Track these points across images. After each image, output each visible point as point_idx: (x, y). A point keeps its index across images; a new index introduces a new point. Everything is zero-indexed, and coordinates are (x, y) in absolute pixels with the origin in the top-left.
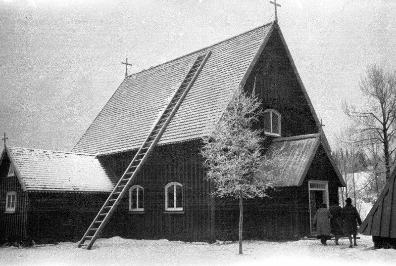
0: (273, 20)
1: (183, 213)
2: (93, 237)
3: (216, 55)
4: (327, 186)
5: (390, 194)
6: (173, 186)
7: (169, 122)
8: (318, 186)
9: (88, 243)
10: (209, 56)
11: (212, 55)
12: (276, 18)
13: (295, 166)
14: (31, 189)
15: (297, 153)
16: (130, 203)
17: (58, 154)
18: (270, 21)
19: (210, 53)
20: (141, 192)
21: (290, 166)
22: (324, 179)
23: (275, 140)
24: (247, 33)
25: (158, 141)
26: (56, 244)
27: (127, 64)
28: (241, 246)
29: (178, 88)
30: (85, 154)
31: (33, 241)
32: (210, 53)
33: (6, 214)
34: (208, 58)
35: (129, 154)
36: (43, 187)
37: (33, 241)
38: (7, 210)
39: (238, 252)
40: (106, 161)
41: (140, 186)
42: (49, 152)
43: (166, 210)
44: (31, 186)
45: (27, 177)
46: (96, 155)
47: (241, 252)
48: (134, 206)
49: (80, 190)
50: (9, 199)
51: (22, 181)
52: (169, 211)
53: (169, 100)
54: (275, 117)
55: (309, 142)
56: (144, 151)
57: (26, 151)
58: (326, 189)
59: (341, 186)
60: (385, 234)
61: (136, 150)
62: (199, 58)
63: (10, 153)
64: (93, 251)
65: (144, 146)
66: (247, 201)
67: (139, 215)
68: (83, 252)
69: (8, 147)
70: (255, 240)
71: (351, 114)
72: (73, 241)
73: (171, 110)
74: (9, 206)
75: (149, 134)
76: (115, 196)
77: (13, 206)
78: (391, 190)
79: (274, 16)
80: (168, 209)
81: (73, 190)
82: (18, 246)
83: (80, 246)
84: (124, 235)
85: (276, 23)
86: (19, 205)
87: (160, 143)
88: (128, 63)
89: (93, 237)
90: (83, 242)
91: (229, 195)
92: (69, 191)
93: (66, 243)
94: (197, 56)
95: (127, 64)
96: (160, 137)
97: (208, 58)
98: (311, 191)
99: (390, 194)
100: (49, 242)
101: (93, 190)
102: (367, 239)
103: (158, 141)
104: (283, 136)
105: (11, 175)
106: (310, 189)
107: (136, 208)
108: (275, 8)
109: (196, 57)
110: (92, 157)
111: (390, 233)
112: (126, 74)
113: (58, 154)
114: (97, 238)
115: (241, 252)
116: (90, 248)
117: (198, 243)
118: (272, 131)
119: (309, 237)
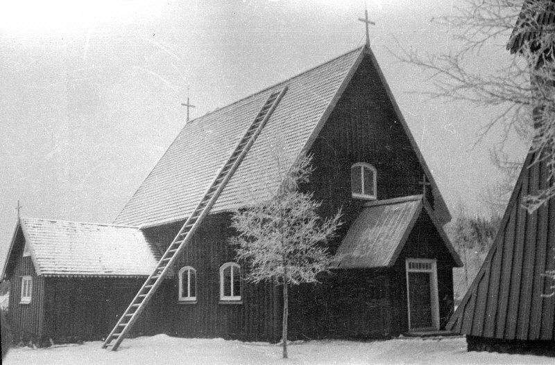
0: (363, 43)
1: (241, 303)
2: (120, 335)
3: (297, 89)
4: (435, 266)
5: (487, 277)
6: (230, 267)
7: (226, 183)
8: (420, 266)
9: (114, 342)
10: (284, 93)
11: (288, 92)
12: (368, 41)
13: (387, 240)
14: (47, 273)
15: (391, 222)
16: (181, 290)
17: (88, 226)
18: (360, 46)
19: (287, 89)
20: (192, 275)
21: (382, 239)
22: (431, 257)
23: (369, 204)
24: (333, 61)
25: (211, 207)
26: (81, 343)
27: (188, 106)
28: (528, 337)
29: (242, 136)
30: (119, 225)
31: (51, 340)
32: (287, 89)
33: (22, 305)
34: (282, 96)
35: (176, 226)
36: (63, 269)
37: (51, 340)
38: (22, 300)
39: (282, 355)
40: (158, 236)
41: (192, 268)
42: (77, 224)
43: (222, 299)
44: (46, 269)
45: (43, 257)
46: (140, 227)
47: (285, 356)
48: (185, 295)
49: (112, 273)
50: (25, 285)
51: (36, 262)
52: (225, 301)
53: (231, 152)
54: (369, 174)
55: (410, 206)
56: (192, 221)
57: (45, 224)
58: (434, 270)
59: (457, 266)
60: (477, 333)
61: (184, 221)
62: (272, 96)
63: (24, 229)
64: (120, 353)
65: (193, 216)
66: (293, 290)
67: (190, 306)
68: (108, 354)
69: (21, 218)
70: (336, 339)
71: (502, 165)
72: (99, 339)
73: (229, 167)
74: (24, 296)
75: (201, 199)
76: (153, 281)
77: (28, 295)
78: (488, 273)
79: (365, 37)
80: (223, 298)
81: (104, 273)
82: (32, 347)
83: (105, 347)
84: (173, 333)
85: (367, 47)
86: (35, 295)
87: (212, 210)
88: (190, 104)
89: (120, 335)
90: (109, 342)
91: (268, 280)
92: (98, 275)
93: (94, 342)
94: (270, 94)
95: (188, 106)
96: (213, 203)
97: (282, 96)
98: (409, 273)
99: (487, 277)
100: (73, 341)
101: (137, 274)
102: (463, 341)
103: (211, 207)
104: (379, 198)
105: (25, 255)
106: (408, 270)
107: (187, 296)
108: (367, 28)
109: (270, 93)
110: (134, 230)
111: (495, 333)
112: (188, 119)
113: (88, 226)
114: (124, 337)
115: (285, 356)
116: (115, 349)
117: (258, 343)
118: (363, 192)
119: (404, 335)
